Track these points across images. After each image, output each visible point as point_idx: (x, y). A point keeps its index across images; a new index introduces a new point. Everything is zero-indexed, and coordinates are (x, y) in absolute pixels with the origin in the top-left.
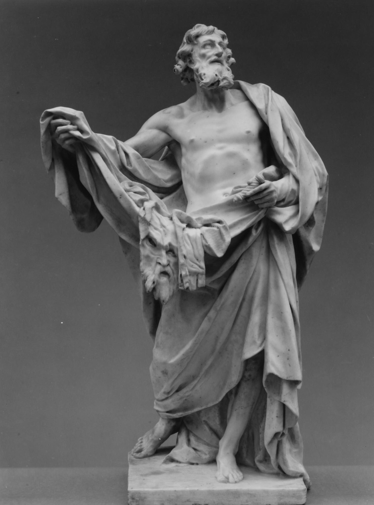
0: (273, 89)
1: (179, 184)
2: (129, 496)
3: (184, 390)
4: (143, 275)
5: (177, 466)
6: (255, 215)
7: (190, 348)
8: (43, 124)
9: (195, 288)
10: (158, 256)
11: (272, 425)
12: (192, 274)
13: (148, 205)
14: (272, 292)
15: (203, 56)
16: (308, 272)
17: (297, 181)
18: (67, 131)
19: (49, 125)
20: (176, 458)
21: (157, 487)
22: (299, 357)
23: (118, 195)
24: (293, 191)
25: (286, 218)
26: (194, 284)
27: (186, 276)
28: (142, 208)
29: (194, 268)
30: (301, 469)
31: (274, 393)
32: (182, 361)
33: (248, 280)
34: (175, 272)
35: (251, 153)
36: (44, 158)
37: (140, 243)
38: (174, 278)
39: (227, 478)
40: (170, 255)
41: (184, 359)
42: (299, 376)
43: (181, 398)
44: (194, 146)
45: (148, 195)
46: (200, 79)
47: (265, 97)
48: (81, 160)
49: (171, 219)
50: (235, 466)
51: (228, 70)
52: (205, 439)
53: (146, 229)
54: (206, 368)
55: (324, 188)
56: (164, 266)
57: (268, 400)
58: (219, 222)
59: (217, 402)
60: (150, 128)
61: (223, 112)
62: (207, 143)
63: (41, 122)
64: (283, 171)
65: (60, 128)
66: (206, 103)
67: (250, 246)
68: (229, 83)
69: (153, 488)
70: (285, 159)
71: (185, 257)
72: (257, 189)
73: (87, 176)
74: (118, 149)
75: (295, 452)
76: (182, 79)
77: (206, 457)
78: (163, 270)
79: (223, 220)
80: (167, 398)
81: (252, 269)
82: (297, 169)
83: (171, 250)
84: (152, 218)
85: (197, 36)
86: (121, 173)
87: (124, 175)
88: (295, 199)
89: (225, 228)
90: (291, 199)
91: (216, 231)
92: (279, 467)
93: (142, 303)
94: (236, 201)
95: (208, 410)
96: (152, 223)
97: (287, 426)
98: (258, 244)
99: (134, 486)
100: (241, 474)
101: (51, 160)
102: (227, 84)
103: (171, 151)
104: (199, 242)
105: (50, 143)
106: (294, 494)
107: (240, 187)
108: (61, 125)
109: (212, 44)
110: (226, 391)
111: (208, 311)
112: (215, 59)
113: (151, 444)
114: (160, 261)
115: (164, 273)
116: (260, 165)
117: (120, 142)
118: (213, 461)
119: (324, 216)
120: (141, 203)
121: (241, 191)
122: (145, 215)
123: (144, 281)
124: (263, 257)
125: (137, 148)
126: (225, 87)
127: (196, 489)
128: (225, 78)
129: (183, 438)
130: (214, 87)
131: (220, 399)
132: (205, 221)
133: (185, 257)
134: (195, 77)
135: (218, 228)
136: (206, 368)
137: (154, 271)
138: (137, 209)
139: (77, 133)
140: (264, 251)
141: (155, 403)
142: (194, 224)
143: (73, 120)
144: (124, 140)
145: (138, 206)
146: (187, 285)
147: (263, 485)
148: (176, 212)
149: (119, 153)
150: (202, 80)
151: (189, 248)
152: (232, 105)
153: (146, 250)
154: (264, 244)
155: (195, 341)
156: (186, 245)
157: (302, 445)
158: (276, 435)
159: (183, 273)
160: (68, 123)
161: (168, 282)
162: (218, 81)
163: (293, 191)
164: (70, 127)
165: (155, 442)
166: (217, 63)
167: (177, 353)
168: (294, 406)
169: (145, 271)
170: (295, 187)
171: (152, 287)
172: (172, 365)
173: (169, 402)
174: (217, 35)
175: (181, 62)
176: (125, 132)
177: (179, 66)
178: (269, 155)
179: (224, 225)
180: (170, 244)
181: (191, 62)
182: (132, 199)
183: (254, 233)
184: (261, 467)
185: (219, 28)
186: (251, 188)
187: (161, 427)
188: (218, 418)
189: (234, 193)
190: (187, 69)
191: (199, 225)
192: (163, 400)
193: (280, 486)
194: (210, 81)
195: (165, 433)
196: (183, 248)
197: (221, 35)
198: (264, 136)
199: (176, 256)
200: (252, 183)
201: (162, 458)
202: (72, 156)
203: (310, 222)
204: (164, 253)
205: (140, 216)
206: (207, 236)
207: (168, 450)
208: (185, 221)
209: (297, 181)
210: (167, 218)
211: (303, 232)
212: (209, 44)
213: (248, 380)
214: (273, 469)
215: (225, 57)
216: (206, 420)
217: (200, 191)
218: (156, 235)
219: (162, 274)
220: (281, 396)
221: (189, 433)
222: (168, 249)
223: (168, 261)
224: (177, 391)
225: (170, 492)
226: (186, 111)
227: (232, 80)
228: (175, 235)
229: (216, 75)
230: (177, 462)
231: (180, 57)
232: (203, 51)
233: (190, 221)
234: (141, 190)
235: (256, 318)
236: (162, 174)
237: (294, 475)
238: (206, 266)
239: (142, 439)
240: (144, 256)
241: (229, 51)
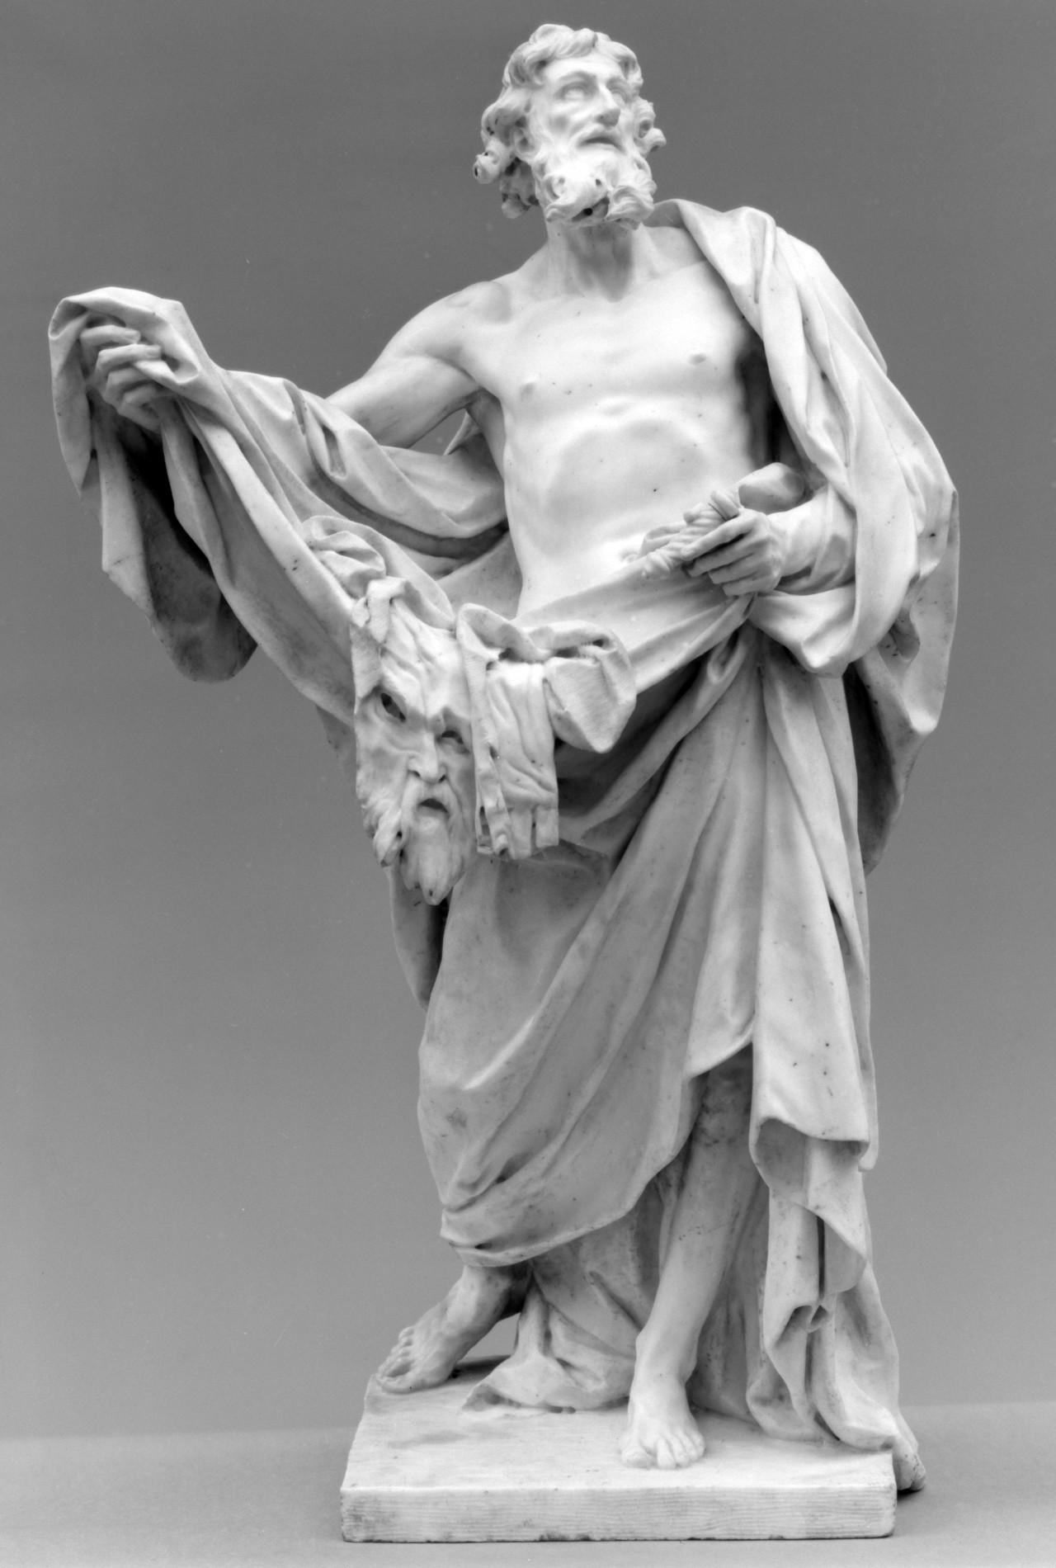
0: (780, 223)
1: (502, 528)
2: (345, 1509)
3: (520, 1177)
4: (367, 812)
5: (507, 1416)
6: (714, 616)
7: (528, 1042)
8: (56, 342)
9: (526, 852)
10: (411, 752)
11: (785, 1283)
12: (514, 805)
13: (380, 589)
14: (776, 863)
15: (560, 124)
16: (902, 799)
17: (850, 511)
18: (127, 364)
19: (78, 342)
20: (505, 1391)
21: (430, 1481)
22: (864, 1066)
23: (285, 559)
24: (836, 540)
25: (814, 628)
26: (524, 837)
27: (499, 812)
28: (362, 600)
29: (521, 786)
30: (888, 1423)
31: (788, 1183)
32: (503, 1082)
33: (701, 824)
34: (465, 800)
35: (712, 424)
36: (65, 448)
37: (356, 710)
38: (464, 820)
39: (652, 1453)
40: (449, 747)
41: (512, 1076)
42: (860, 1124)
43: (516, 1202)
44: (538, 406)
45: (381, 560)
46: (547, 196)
47: (754, 249)
49: (453, 632)
50: (682, 1414)
51: (640, 166)
52: (595, 1332)
53: (374, 667)
54: (580, 1104)
55: (943, 536)
56: (430, 783)
57: (773, 1204)
58: (600, 642)
59: (620, 1214)
60: (408, 353)
62: (575, 396)
63: (52, 337)
64: (806, 482)
65: (107, 354)
66: (574, 272)
67: (705, 719)
68: (639, 205)
69: (418, 1484)
70: (812, 442)
72: (713, 536)
73: (192, 503)
74: (302, 420)
75: (871, 1372)
76: (505, 197)
77: (596, 1387)
78: (426, 794)
79: (611, 637)
80: (471, 1203)
81: (715, 787)
82: (848, 475)
83: (450, 734)
84: (390, 633)
85: (542, 63)
86: (311, 493)
87: (320, 501)
88: (845, 566)
89: (617, 659)
90: (832, 566)
91: (590, 670)
92: (819, 1420)
93: (391, 904)
94: (648, 577)
95: (601, 1236)
96: (392, 646)
97: (834, 1287)
98: (729, 711)
99: (364, 1477)
100: (698, 1439)
101: (88, 454)
102: (632, 209)
103: (471, 427)
104: (537, 703)
105: (82, 403)
106: (856, 1504)
107: (667, 531)
108: (112, 343)
109: (586, 85)
110: (645, 1175)
111: (583, 924)
112: (595, 132)
113: (437, 1348)
114: (419, 769)
115: (431, 805)
116: (740, 461)
117: (308, 397)
118: (620, 1401)
119: (949, 620)
120: (358, 585)
121: (667, 543)
122: (368, 622)
123: (372, 831)
124: (745, 752)
125: (363, 417)
126: (627, 220)
127: (551, 1486)
128: (624, 192)
129: (529, 1325)
130: (594, 220)
131: (630, 1203)
132: (558, 638)
133: (493, 753)
134: (537, 191)
135: (596, 660)
136: (580, 1104)
137: (401, 798)
138: (347, 603)
139: (160, 369)
140: (749, 730)
141: (443, 1219)
142: (523, 650)
143: (145, 326)
144: (325, 390)
145: (352, 595)
146: (500, 842)
147: (764, 1475)
148: (469, 613)
149: (304, 431)
150: (555, 196)
151: (507, 723)
152: (653, 275)
153: (374, 731)
154: (751, 713)
155: (542, 1018)
156: (497, 714)
157: (892, 1347)
158: (798, 1313)
159: (489, 804)
160: (131, 337)
161: (445, 833)
162: (605, 201)
163: (837, 543)
164: (136, 348)
165: (449, 1341)
166: (602, 145)
167: (490, 1058)
168: (851, 1225)
169: (372, 800)
170: (843, 529)
171: (395, 848)
172: (474, 1095)
173: (477, 1213)
174: (605, 57)
175: (494, 145)
176: (329, 363)
177: (491, 158)
178: (771, 433)
179: (614, 650)
180: (447, 714)
182: (330, 573)
183: (714, 677)
184: (766, 1417)
185: (614, 37)
186: (693, 533)
187: (467, 1296)
188: (632, 1265)
189: (647, 549)
190: (515, 166)
191: (542, 652)
192: (462, 1208)
193: (816, 1477)
194: (579, 200)
195: (479, 1315)
196: (487, 725)
197: (618, 57)
198: (752, 368)
199: (466, 751)
200: (698, 517)
201: (465, 1391)
202: (150, 442)
203: (898, 639)
204: (428, 739)
205: (354, 626)
206: (562, 686)
207: (485, 1367)
208: (498, 640)
209: (850, 511)
210: (443, 633)
211: (878, 673)
213: (716, 1142)
215: (629, 127)
216: (599, 1271)
217: (554, 548)
218: (402, 684)
219: (425, 809)
220: (806, 1192)
221: (548, 1309)
222: (443, 730)
223: (443, 765)
224: (501, 1179)
225: (469, 1496)
226: (517, 301)
227: (650, 198)
228: (463, 681)
229: (598, 182)
231: (493, 128)
232: (560, 108)
233: (513, 642)
234: (360, 543)
235: (725, 946)
236: (445, 496)
237: (862, 1444)
238: (560, 781)
239: (411, 1333)
240: (367, 750)
241: (646, 108)
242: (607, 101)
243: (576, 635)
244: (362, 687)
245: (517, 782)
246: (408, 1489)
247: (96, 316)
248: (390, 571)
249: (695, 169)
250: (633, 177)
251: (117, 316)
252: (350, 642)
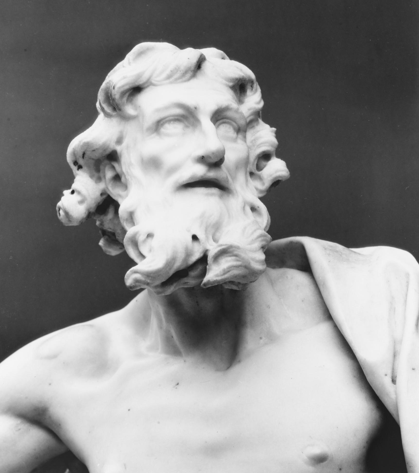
15: (153, 164)
47: (392, 309)
61: (236, 369)
85: (136, 90)
109: (188, 116)
177: (75, 202)
185: (233, 54)
190: (107, 204)
212: (178, 119)
229: (195, 238)
231: (81, 162)
242: (210, 138)
250: (238, 228)
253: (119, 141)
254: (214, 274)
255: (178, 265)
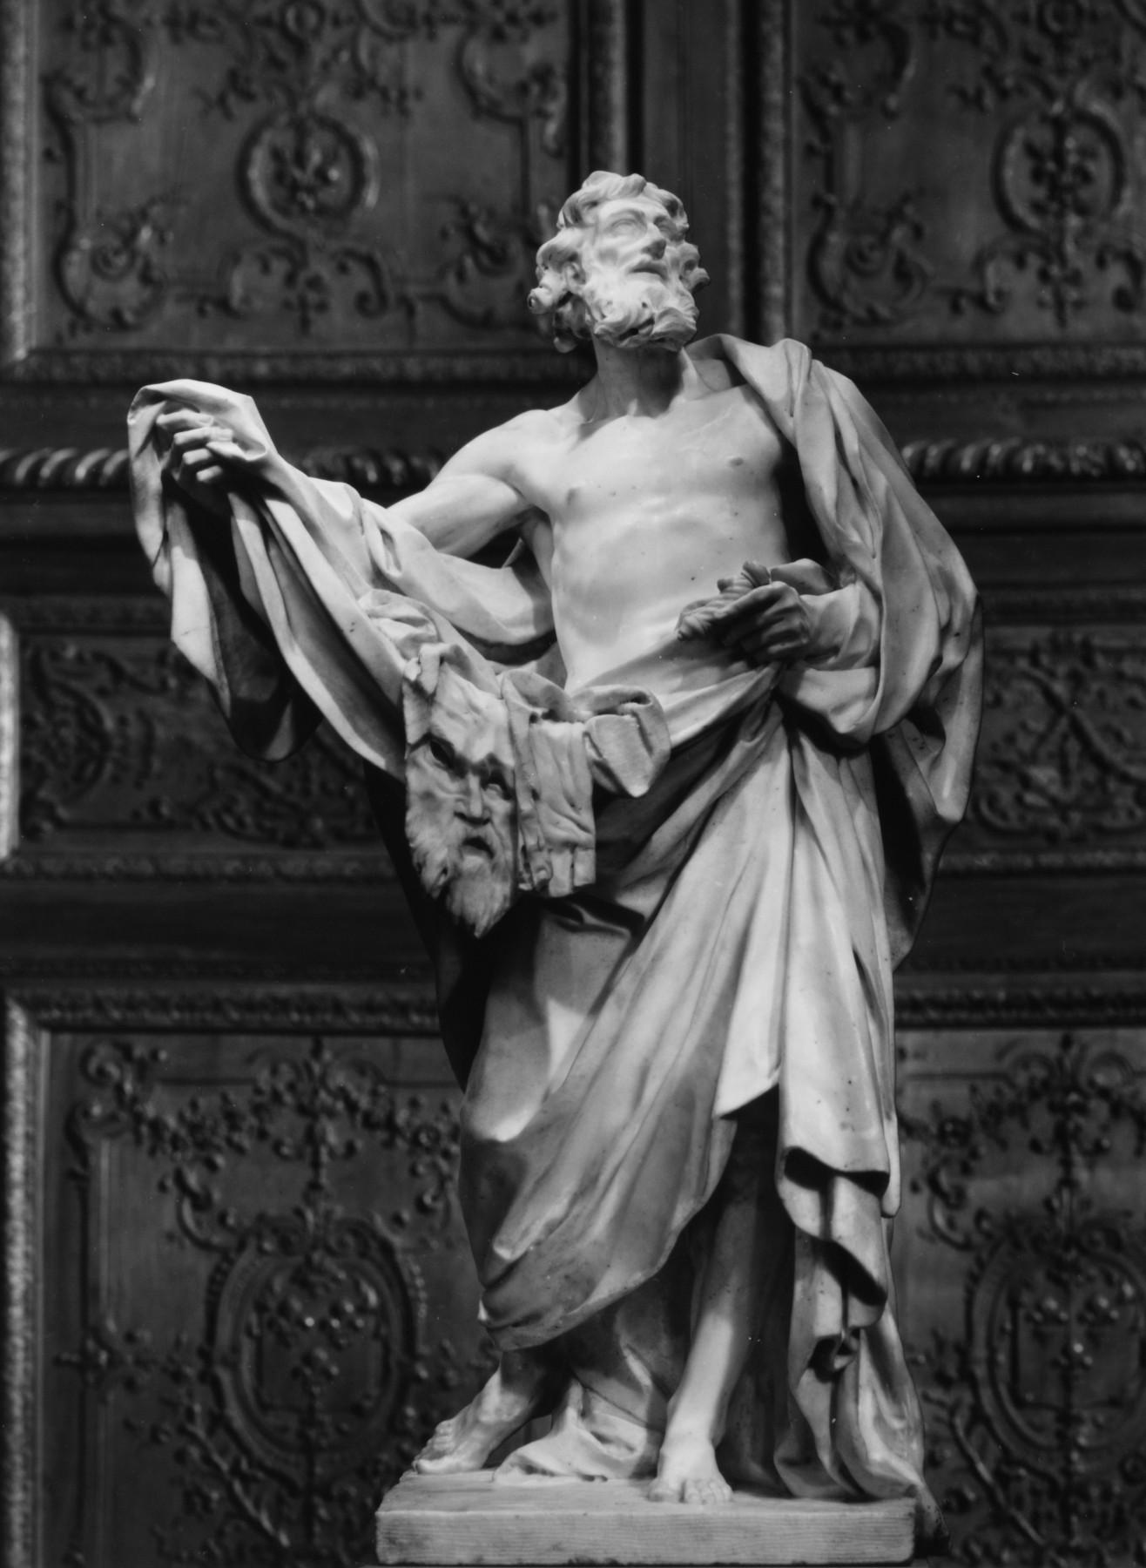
18: (200, 443)
28: (414, 660)
48: (246, 529)
51: (683, 295)
64: (835, 568)
69: (452, 1510)
71: (535, 795)
72: (744, 599)
83: (492, 774)
92: (844, 1471)
115: (477, 844)
133: (535, 795)
135: (634, 714)
139: (230, 450)
145: (405, 657)
178: (801, 528)
180: (492, 759)
181: (580, 277)
184: (790, 1478)
204: (474, 782)
205: (406, 679)
212: (628, 222)
214: (830, 1481)
215: (675, 263)
218: (456, 736)
229: (644, 305)
230: (544, 1472)
236: (501, 600)
243: (614, 695)
244: (413, 733)
245: (556, 824)
246: (442, 1514)
247: (174, 402)
248: (439, 639)
249: (733, 306)
250: (672, 302)
251: (193, 403)
252: (401, 696)
253: (580, 245)
254: (658, 328)
255: (632, 322)
